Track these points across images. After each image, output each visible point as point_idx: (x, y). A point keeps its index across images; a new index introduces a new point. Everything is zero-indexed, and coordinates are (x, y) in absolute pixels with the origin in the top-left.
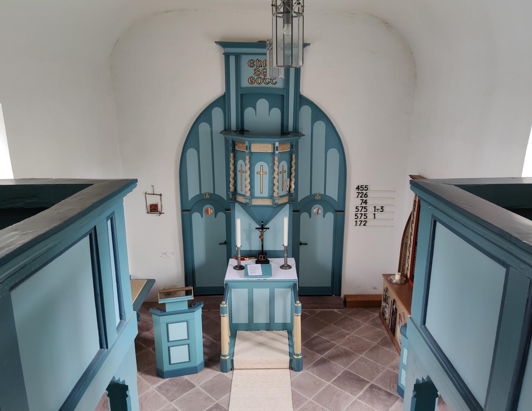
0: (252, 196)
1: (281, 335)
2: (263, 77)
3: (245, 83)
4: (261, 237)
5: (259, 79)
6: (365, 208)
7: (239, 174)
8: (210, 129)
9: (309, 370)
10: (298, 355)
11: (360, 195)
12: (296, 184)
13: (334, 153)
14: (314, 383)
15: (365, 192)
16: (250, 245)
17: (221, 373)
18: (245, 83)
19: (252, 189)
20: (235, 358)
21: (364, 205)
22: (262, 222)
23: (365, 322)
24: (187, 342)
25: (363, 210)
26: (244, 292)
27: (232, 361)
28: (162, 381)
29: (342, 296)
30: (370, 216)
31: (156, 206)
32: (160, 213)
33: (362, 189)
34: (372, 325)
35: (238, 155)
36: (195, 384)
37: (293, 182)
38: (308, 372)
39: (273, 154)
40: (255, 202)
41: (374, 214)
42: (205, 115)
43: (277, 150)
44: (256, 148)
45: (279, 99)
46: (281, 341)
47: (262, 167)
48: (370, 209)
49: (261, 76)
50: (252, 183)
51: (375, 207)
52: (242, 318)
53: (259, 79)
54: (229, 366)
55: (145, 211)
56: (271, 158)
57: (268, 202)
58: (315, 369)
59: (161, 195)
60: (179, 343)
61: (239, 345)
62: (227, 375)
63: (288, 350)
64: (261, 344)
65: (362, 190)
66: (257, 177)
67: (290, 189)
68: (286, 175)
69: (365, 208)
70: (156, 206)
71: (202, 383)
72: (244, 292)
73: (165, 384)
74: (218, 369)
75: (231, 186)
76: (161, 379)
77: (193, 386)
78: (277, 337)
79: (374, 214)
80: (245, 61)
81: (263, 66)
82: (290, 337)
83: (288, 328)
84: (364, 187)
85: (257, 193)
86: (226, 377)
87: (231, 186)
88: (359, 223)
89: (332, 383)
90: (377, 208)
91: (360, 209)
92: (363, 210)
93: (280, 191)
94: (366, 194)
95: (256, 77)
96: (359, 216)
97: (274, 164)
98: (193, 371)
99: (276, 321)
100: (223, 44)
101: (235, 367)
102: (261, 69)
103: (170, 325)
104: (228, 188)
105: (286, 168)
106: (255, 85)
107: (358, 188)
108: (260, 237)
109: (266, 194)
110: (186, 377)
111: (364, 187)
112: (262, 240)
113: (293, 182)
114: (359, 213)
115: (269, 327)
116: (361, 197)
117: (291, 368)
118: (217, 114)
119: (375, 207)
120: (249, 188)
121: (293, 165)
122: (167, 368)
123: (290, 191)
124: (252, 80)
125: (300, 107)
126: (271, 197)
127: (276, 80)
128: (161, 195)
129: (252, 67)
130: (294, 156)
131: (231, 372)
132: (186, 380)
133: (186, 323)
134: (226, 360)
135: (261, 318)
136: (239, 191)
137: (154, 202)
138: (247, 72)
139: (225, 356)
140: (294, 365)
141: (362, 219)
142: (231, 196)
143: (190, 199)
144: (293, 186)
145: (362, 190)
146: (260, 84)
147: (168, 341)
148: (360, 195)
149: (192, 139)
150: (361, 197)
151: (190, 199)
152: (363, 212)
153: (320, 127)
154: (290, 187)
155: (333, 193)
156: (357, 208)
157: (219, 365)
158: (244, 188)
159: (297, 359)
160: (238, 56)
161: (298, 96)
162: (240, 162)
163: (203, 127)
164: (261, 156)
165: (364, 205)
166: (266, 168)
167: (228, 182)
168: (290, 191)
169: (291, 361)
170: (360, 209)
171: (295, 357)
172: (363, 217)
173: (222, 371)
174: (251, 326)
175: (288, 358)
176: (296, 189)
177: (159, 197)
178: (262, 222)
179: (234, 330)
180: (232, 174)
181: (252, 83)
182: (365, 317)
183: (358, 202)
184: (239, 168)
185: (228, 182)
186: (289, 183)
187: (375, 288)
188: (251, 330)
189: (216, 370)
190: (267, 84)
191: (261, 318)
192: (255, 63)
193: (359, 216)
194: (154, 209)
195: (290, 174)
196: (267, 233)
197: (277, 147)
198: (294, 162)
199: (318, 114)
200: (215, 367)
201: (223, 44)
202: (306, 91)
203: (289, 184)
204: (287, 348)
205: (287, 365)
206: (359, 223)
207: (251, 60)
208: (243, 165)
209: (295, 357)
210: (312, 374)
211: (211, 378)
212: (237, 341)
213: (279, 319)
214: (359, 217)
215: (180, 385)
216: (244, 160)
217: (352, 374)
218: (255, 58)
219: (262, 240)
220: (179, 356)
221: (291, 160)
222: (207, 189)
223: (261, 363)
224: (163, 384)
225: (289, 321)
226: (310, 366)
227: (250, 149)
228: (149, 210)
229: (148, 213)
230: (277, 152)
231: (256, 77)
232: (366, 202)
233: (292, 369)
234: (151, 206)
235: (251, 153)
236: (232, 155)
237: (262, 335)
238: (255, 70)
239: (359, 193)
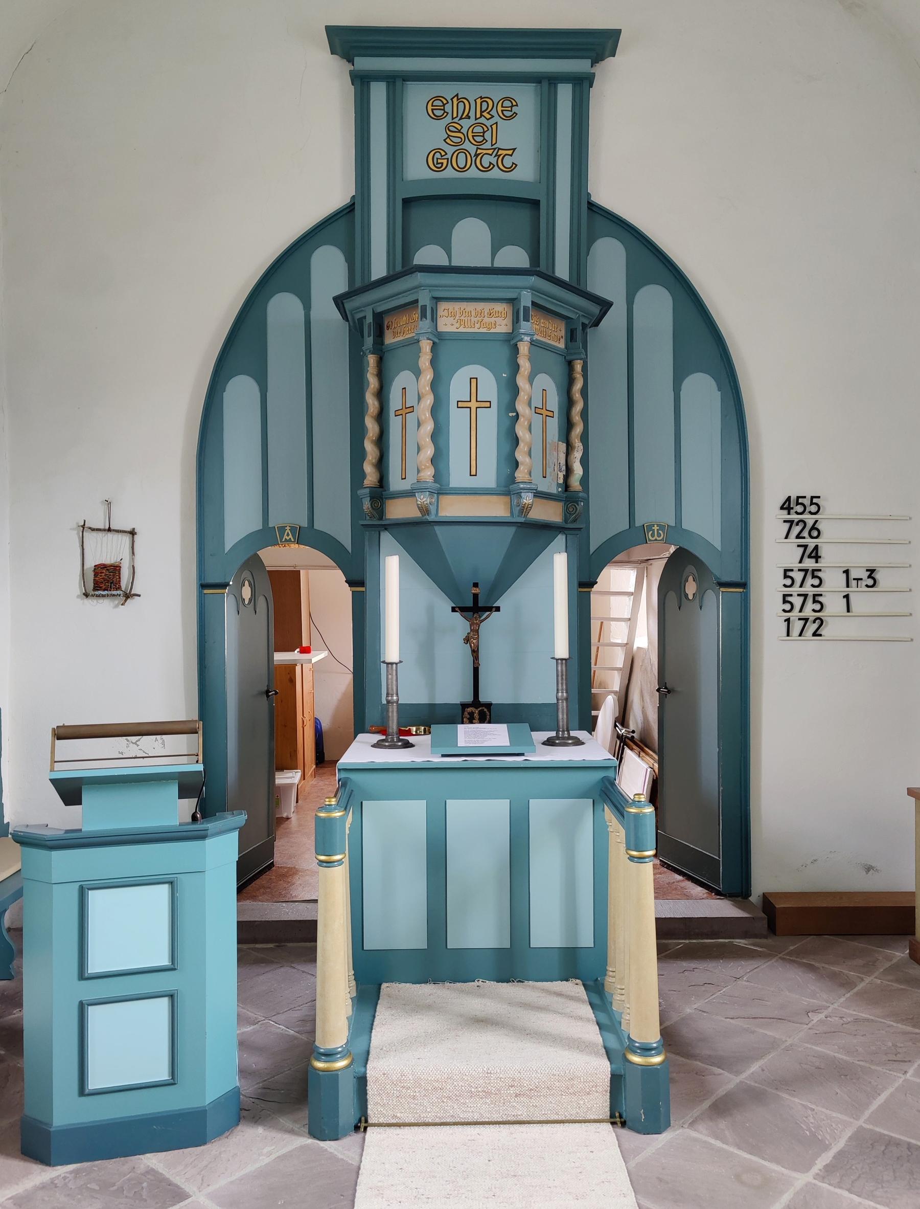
0: (441, 488)
1: (559, 994)
2: (472, 149)
3: (417, 169)
4: (472, 641)
5: (462, 157)
6: (814, 573)
7: (395, 424)
8: (302, 313)
9: (701, 1127)
10: (646, 1050)
11: (796, 530)
12: (585, 462)
13: (701, 389)
14: (738, 1177)
15: (810, 519)
16: (431, 684)
17: (310, 1141)
18: (417, 169)
19: (439, 459)
20: (373, 1070)
21: (809, 563)
22: (476, 585)
23: (869, 973)
24: (163, 983)
25: (810, 581)
26: (412, 813)
27: (362, 1081)
28: (40, 1175)
29: (754, 898)
30: (833, 604)
31: (115, 569)
32: (128, 596)
33: (799, 509)
34: (898, 981)
35: (391, 362)
36: (188, 1187)
37: (577, 454)
38: (694, 1134)
39: (511, 341)
40: (452, 508)
41: (847, 597)
42: (286, 270)
43: (526, 319)
44: (451, 319)
45: (520, 211)
46: (565, 1010)
47: (474, 381)
48: (833, 581)
49: (467, 145)
50: (438, 435)
51: (847, 572)
52: (400, 924)
53: (462, 157)
54: (347, 1112)
55: (75, 587)
56: (504, 352)
57: (496, 508)
58: (722, 1124)
59: (133, 533)
60: (129, 985)
61: (389, 1027)
62: (339, 1149)
63: (599, 1040)
64: (482, 1022)
65: (801, 513)
66: (458, 420)
67: (567, 477)
68: (554, 425)
69: (814, 573)
70: (115, 569)
71: (223, 1182)
72: (412, 813)
73: (52, 1185)
74: (296, 1127)
75: (369, 468)
76: (36, 1168)
77: (179, 1195)
78: (545, 1000)
79: (847, 597)
80: (417, 98)
81: (472, 114)
82: (597, 1001)
83: (586, 968)
84: (807, 502)
85: (458, 477)
86: (333, 1158)
87: (369, 468)
88: (797, 626)
89: (820, 1177)
90: (854, 574)
91: (798, 577)
92: (810, 581)
93: (540, 467)
94: (813, 528)
95: (450, 150)
96: (797, 601)
97: (516, 368)
98: (185, 1130)
99: (537, 941)
100: (348, 42)
101: (374, 1113)
102: (466, 124)
103: (94, 897)
104: (357, 475)
105: (554, 402)
106: (449, 173)
107: (787, 506)
108: (467, 640)
109: (488, 477)
110: (152, 1161)
111: (807, 502)
112: (475, 653)
113: (577, 454)
114: (796, 589)
115: (511, 964)
116: (798, 537)
117: (618, 1118)
118: (329, 271)
119: (847, 572)
120: (429, 451)
121: (577, 396)
122: (66, 1112)
123: (566, 486)
124: (437, 160)
125: (591, 241)
126: (508, 487)
127: (515, 158)
128: (133, 533)
129: (438, 118)
130: (578, 366)
131: (352, 1139)
132: (151, 1171)
133: (165, 889)
134: (333, 1076)
135: (478, 928)
136: (396, 483)
137: (108, 559)
138: (424, 135)
139: (329, 1055)
140: (632, 1105)
141: (808, 612)
142: (367, 504)
143: (228, 546)
144: (578, 470)
145: (801, 513)
146: (462, 170)
147: (82, 975)
148: (796, 530)
149: (242, 345)
150: (798, 537)
151: (228, 546)
152: (808, 589)
153: (656, 306)
154: (569, 471)
155: (705, 523)
156: (786, 573)
157: (304, 1114)
158: (411, 464)
159: (648, 1071)
160: (396, 82)
161: (585, 206)
162: (402, 380)
163: (283, 308)
164: (473, 345)
165: (809, 563)
166: (489, 388)
167: (357, 455)
168: (566, 486)
169: (616, 1081)
170: (798, 577)
171: (636, 1059)
172: (810, 606)
173: (317, 1133)
174: (440, 962)
175: (603, 1068)
176: (585, 480)
177: (127, 539)
178: (476, 585)
179: (373, 975)
180: (371, 426)
181: (439, 168)
182: (860, 962)
183: (790, 555)
184: (395, 402)
185: (357, 455)
186: (562, 457)
187: (869, 869)
188: (435, 981)
189: (291, 1132)
190: (487, 169)
191: (478, 928)
192: (448, 108)
193: (797, 601)
194: (106, 581)
195: (568, 426)
196: (492, 624)
197: (526, 309)
198: (578, 385)
199: (652, 262)
200: (284, 1121)
201: (348, 42)
202: (606, 192)
203: (563, 462)
204: (593, 1034)
205: (600, 1104)
206: (797, 626)
207: (437, 98)
208: (410, 386)
209: (636, 1059)
210: (718, 1144)
211: (265, 1161)
212: (382, 1013)
213: (546, 932)
214: (797, 606)
215: (121, 1189)
216: (417, 373)
217: (891, 1143)
218: (448, 90)
219: (475, 653)
220: (126, 1049)
221: (571, 381)
222: (289, 511)
223: (488, 1094)
224: (43, 1187)
225: (586, 940)
226: (696, 1112)
227: (434, 319)
228: (90, 585)
229: (86, 595)
230: (525, 327)
231: (450, 150)
232: (815, 555)
233: (624, 1124)
234: (99, 569)
235: (439, 340)
236: (372, 360)
237: (482, 996)
238: (447, 128)
239: (791, 522)
